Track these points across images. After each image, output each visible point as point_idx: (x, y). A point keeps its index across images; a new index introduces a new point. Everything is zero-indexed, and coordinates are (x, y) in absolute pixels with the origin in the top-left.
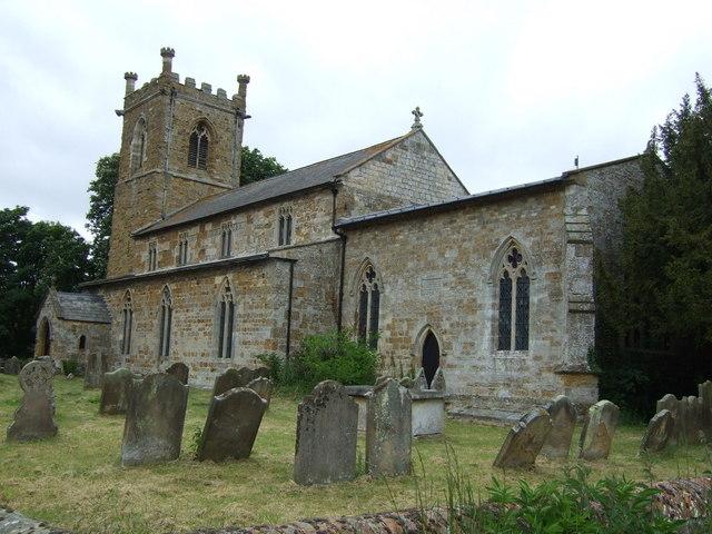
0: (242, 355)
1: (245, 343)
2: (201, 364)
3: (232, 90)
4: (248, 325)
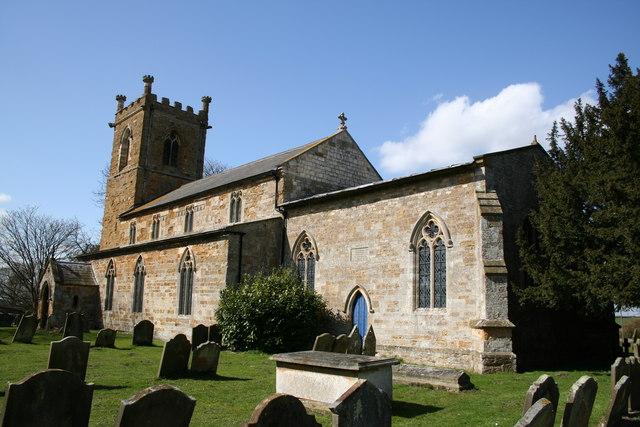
0: (200, 312)
1: (202, 303)
2: (168, 320)
3: (198, 109)
4: (205, 288)
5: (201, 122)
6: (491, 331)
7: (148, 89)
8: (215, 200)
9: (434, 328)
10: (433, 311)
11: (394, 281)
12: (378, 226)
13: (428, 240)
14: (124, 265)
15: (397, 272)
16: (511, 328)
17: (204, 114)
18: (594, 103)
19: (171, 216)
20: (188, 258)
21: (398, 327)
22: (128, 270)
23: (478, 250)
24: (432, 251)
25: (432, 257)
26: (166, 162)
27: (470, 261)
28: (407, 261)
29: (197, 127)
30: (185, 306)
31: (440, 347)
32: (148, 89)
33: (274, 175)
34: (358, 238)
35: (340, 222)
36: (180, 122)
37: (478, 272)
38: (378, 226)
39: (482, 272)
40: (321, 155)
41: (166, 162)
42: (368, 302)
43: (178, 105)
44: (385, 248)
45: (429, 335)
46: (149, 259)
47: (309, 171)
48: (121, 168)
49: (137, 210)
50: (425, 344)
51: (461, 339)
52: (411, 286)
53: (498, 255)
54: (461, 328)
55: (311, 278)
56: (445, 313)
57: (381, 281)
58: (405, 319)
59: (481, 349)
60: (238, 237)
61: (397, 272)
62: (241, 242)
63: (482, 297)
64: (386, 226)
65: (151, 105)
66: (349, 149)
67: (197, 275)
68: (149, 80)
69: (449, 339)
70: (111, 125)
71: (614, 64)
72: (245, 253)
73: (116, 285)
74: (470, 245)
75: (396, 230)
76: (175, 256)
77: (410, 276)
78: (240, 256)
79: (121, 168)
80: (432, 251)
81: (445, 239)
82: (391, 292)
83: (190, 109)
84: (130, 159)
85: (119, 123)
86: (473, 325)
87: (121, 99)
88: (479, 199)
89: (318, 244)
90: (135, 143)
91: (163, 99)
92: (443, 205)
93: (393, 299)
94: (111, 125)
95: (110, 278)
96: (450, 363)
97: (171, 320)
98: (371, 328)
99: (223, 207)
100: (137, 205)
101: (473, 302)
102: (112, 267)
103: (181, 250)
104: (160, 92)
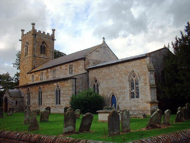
1: (64, 100)
3: (51, 33)
4: (64, 96)
5: (52, 38)
6: (152, 103)
7: (33, 28)
8: (63, 67)
9: (136, 104)
10: (135, 99)
11: (124, 91)
12: (118, 75)
13: (133, 78)
14: (34, 91)
15: (124, 88)
16: (170, 52)
17: (53, 35)
18: (181, 38)
19: (47, 72)
20: (58, 87)
21: (125, 102)
22: (35, 91)
23: (148, 81)
24: (134, 82)
25: (135, 83)
26: (41, 53)
27: (146, 84)
28: (128, 85)
29: (51, 40)
30: (58, 101)
31: (138, 109)
32: (33, 28)
33: (84, 59)
34: (112, 78)
35: (106, 73)
36: (45, 39)
37: (148, 87)
38: (118, 75)
39: (149, 87)
40: (98, 51)
41: (41, 53)
42: (116, 98)
43: (44, 33)
44: (121, 81)
45: (135, 106)
46: (43, 87)
47: (94, 57)
48: (25, 56)
49: (33, 70)
50: (134, 109)
51: (144, 107)
52: (129, 92)
53: (153, 82)
54: (144, 104)
55: (98, 91)
56: (139, 100)
57: (120, 91)
58: (128, 102)
59: (150, 109)
60: (74, 80)
61: (124, 88)
62: (75, 81)
63: (149, 94)
64: (120, 74)
65: (34, 33)
66: (106, 49)
67: (62, 92)
68: (33, 24)
69: (140, 107)
70: (20, 40)
71: (187, 25)
72: (77, 84)
73: (31, 96)
74: (145, 80)
75: (124, 76)
76: (53, 86)
77: (128, 89)
78: (76, 86)
79: (25, 56)
80: (134, 82)
81: (138, 78)
82: (123, 94)
83: (48, 34)
84: (28, 52)
85: (23, 40)
86: (147, 102)
87: (23, 31)
88: (148, 66)
89: (99, 80)
90: (30, 46)
91: (39, 31)
92: (137, 68)
93: (123, 96)
94: (20, 40)
95: (29, 94)
96: (141, 112)
97: (53, 106)
98: (118, 105)
99: (66, 69)
100: (33, 69)
101: (147, 96)
102: (29, 90)
103: (55, 84)
104: (38, 29)
